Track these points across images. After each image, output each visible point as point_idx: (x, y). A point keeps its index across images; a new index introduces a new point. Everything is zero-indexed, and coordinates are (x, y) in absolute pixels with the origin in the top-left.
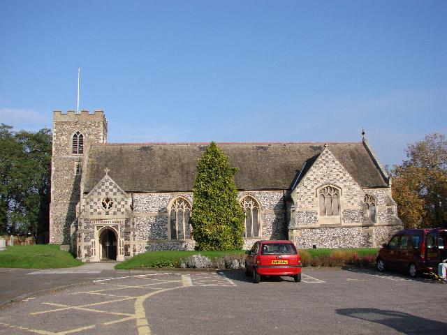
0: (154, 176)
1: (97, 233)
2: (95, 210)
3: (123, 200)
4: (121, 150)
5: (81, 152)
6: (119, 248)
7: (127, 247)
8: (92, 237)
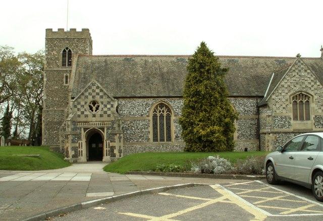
0: (137, 83)
1: (83, 134)
2: (83, 113)
3: (109, 103)
4: (106, 61)
5: (70, 64)
6: (105, 149)
7: (112, 148)
8: (80, 138)
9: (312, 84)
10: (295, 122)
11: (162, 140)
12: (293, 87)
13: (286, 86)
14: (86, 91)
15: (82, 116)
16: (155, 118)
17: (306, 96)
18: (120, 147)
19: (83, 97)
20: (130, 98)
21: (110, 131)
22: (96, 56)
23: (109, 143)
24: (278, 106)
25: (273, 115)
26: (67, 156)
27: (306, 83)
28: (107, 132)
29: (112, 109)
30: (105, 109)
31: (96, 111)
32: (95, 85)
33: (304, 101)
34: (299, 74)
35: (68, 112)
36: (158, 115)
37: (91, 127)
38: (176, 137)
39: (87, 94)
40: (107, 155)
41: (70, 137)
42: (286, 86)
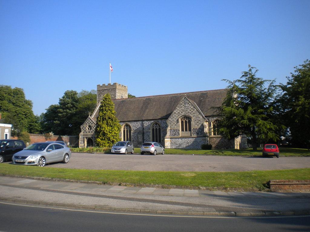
9: (192, 110)
36: (155, 128)
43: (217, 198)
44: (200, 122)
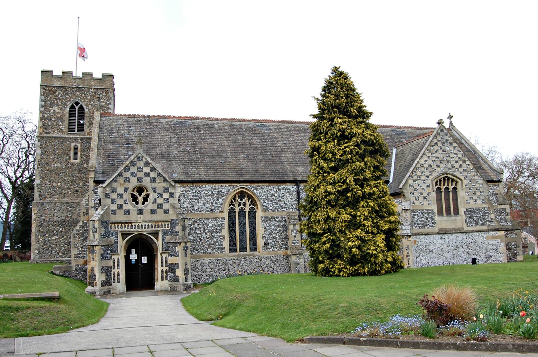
2: (120, 207)
3: (166, 190)
7: (173, 268)
8: (115, 251)
10: (440, 218)
11: (243, 249)
12: (435, 167)
13: (426, 166)
14: (127, 169)
15: (120, 212)
16: (232, 214)
17: (453, 180)
18: (186, 264)
19: (121, 180)
20: (193, 182)
21: (168, 238)
22: (119, 115)
23: (166, 258)
24: (416, 194)
25: (411, 209)
26: (92, 284)
27: (453, 162)
28: (163, 240)
29: (171, 200)
30: (160, 201)
31: (143, 203)
32: (142, 160)
33: (451, 188)
34: (443, 148)
35: (87, 205)
36: (237, 209)
37: (135, 231)
38: (265, 244)
39: (127, 174)
40: (162, 279)
41: (98, 250)
42: (426, 166)
43: (408, 351)
44: (478, 194)
